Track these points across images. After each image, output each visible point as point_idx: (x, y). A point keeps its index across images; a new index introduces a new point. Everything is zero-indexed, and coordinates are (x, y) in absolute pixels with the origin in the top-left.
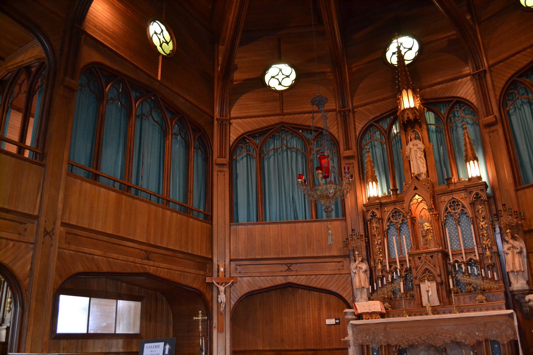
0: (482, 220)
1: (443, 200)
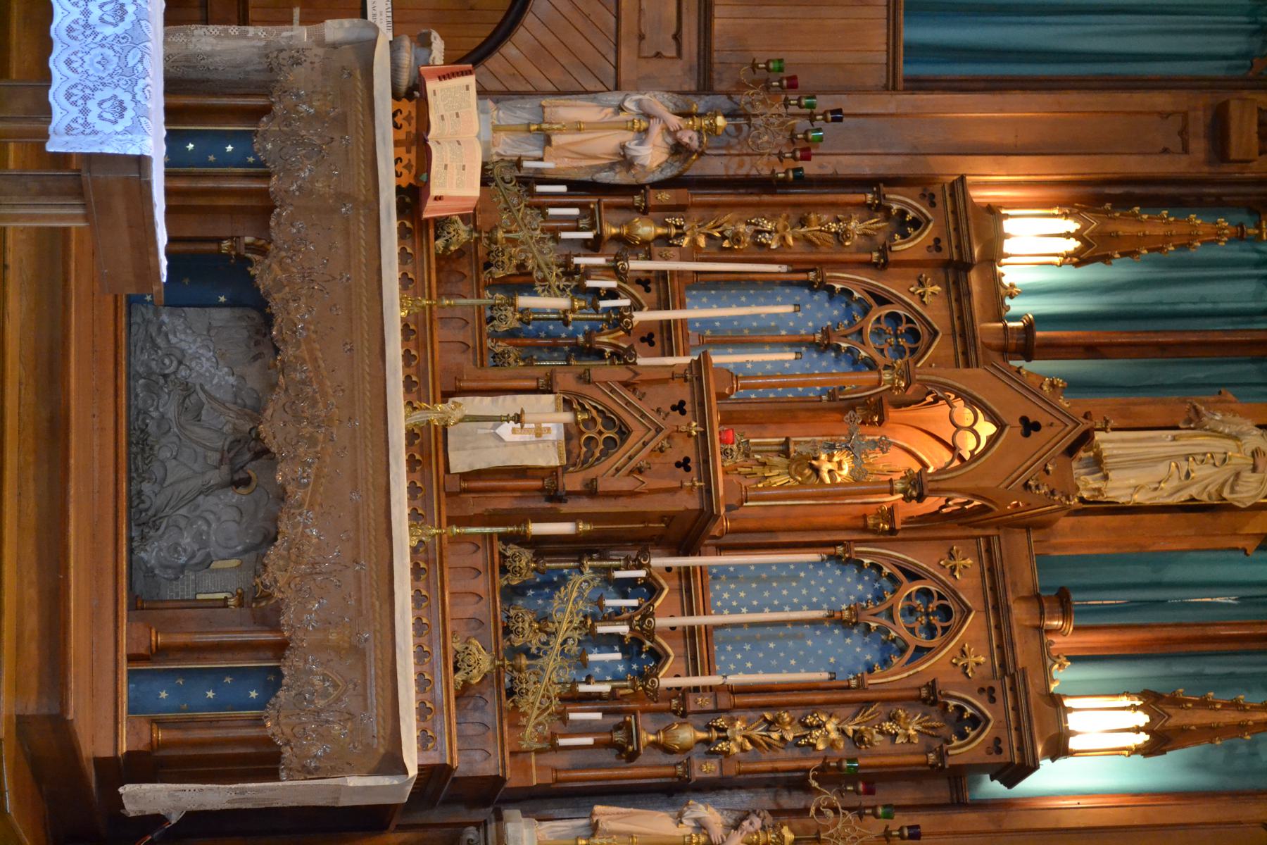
0: (850, 730)
1: (960, 563)
